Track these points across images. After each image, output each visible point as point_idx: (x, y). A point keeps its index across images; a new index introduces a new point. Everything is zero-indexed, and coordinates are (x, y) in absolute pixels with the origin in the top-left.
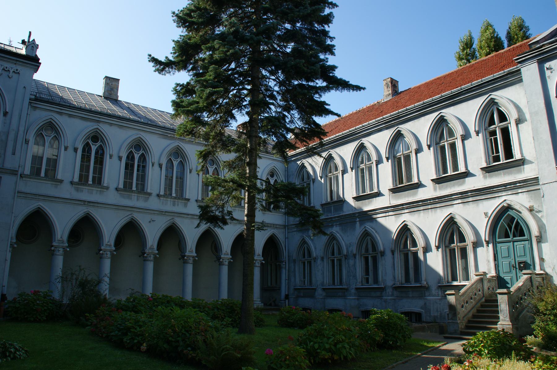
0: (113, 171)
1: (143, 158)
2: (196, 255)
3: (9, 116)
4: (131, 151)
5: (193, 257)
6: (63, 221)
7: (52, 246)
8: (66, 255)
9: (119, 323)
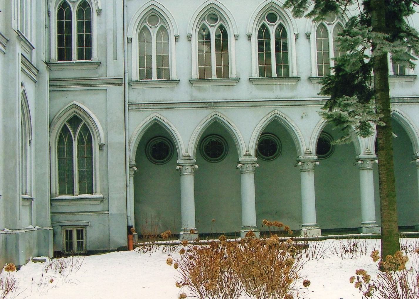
0: (243, 57)
1: (223, 34)
2: (375, 156)
3: (103, 13)
4: (263, 26)
5: (373, 160)
6: (186, 134)
7: (239, 163)
8: (197, 175)
9: (220, 259)
